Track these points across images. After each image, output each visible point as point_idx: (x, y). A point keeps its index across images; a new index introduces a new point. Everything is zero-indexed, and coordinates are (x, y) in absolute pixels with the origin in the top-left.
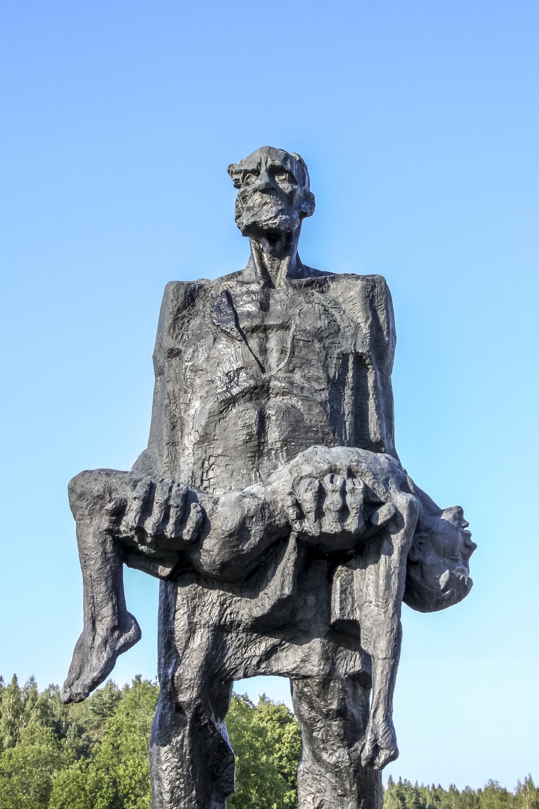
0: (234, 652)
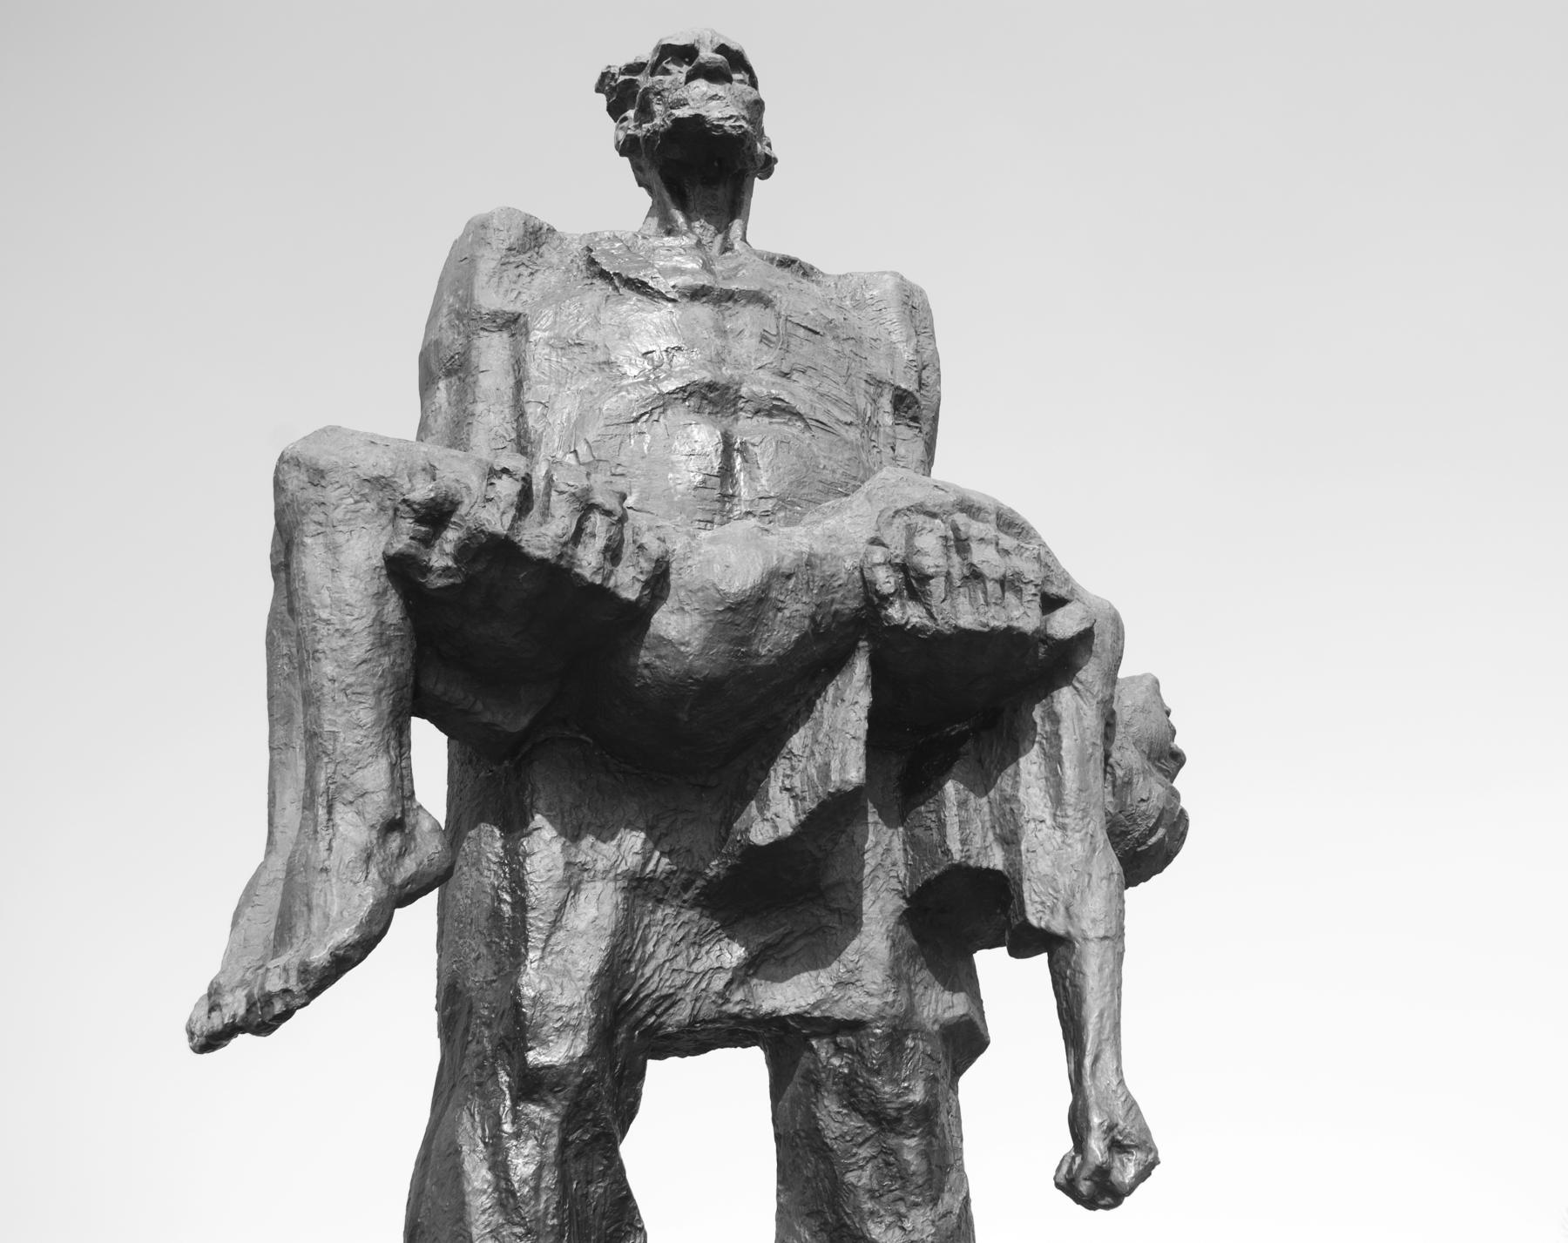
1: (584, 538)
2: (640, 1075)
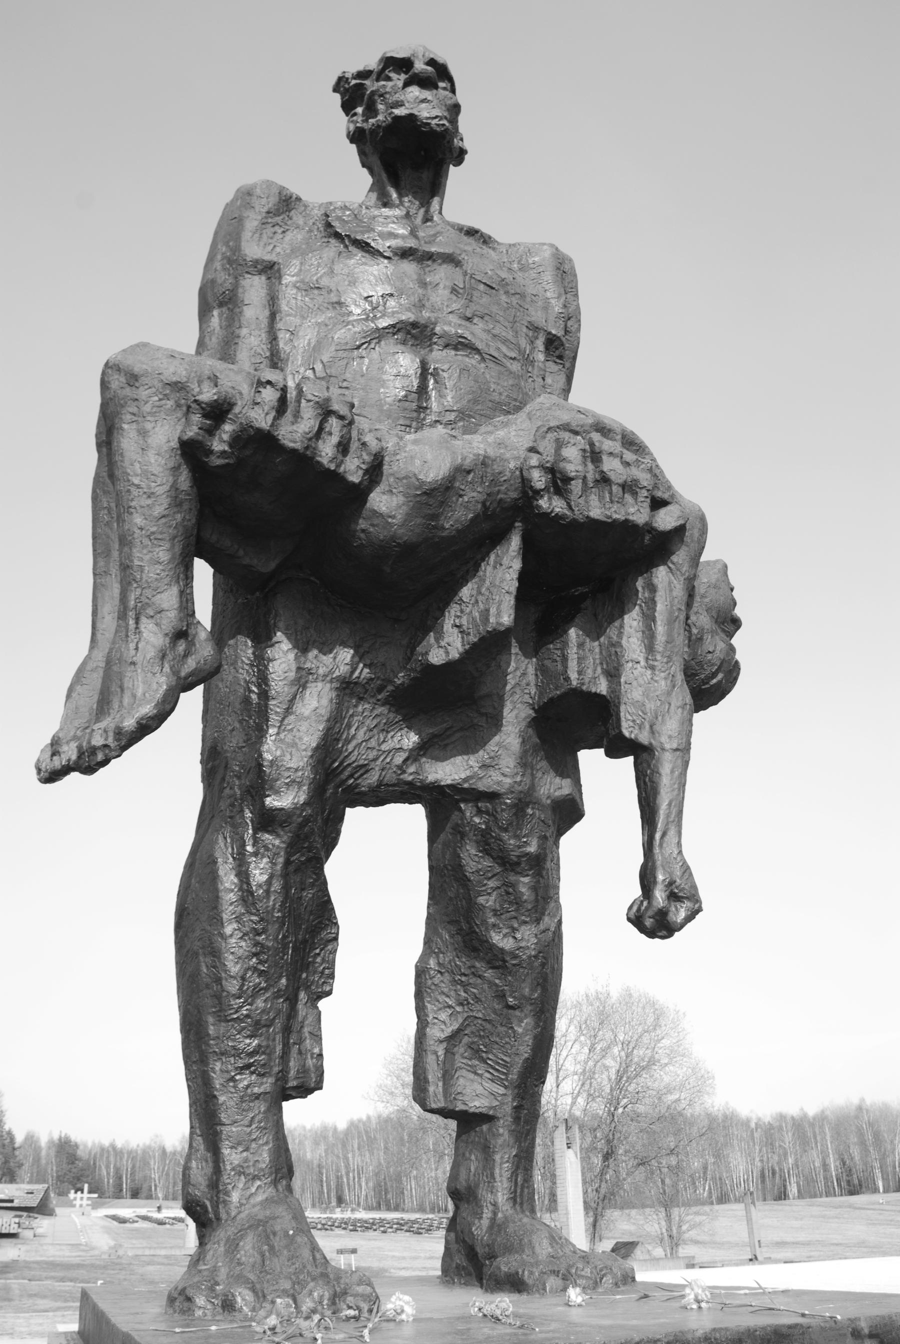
0: (367, 737)
1: (323, 435)
2: (341, 819)
